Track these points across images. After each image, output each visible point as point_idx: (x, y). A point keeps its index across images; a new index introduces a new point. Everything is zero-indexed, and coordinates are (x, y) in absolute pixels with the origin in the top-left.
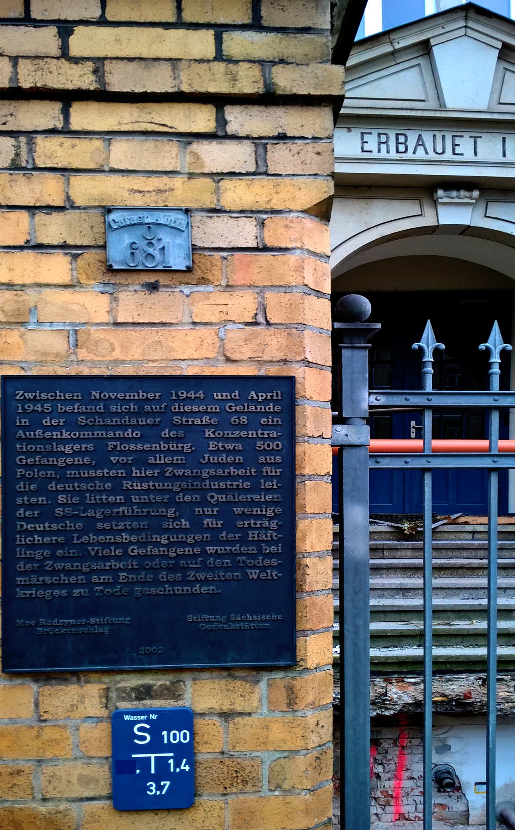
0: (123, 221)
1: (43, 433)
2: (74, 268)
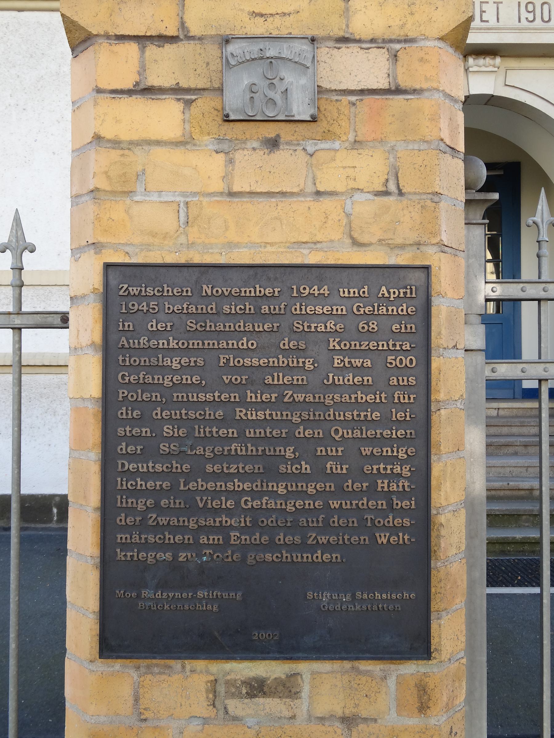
0: (242, 56)
1: (148, 341)
2: (187, 119)
